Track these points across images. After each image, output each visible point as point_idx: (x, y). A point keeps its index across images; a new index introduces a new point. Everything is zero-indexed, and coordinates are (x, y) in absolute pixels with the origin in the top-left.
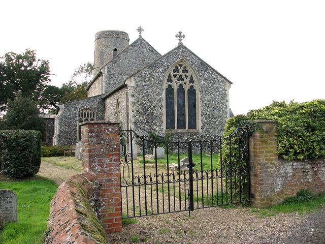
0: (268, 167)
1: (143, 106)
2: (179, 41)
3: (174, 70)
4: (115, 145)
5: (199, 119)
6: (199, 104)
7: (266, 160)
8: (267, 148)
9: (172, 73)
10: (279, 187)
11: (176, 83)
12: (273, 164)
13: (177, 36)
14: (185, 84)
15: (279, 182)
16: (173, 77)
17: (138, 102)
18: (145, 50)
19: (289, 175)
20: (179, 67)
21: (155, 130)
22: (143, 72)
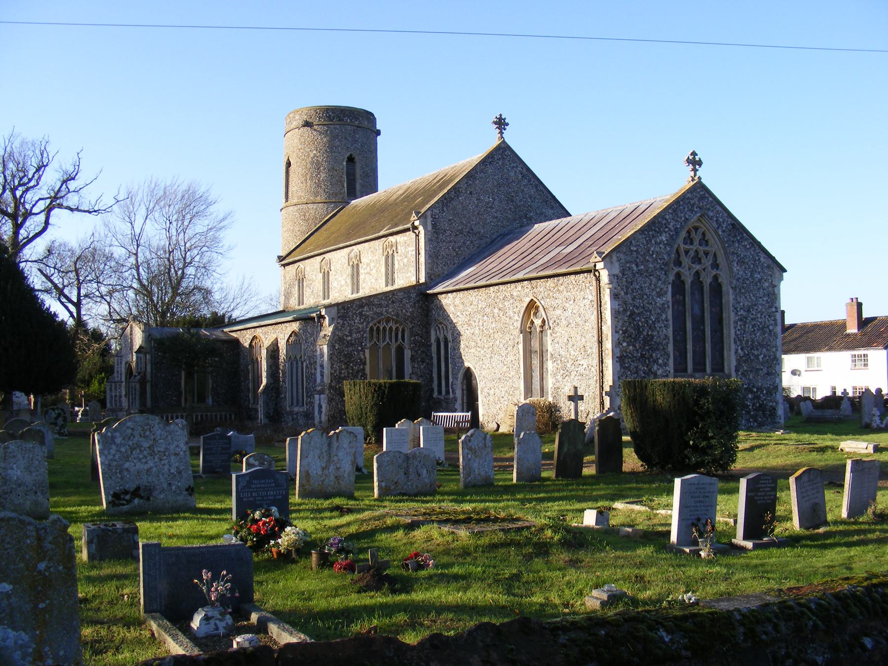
5: (730, 350)
6: (730, 317)
11: (689, 269)
16: (683, 254)
18: (512, 174)
20: (693, 234)
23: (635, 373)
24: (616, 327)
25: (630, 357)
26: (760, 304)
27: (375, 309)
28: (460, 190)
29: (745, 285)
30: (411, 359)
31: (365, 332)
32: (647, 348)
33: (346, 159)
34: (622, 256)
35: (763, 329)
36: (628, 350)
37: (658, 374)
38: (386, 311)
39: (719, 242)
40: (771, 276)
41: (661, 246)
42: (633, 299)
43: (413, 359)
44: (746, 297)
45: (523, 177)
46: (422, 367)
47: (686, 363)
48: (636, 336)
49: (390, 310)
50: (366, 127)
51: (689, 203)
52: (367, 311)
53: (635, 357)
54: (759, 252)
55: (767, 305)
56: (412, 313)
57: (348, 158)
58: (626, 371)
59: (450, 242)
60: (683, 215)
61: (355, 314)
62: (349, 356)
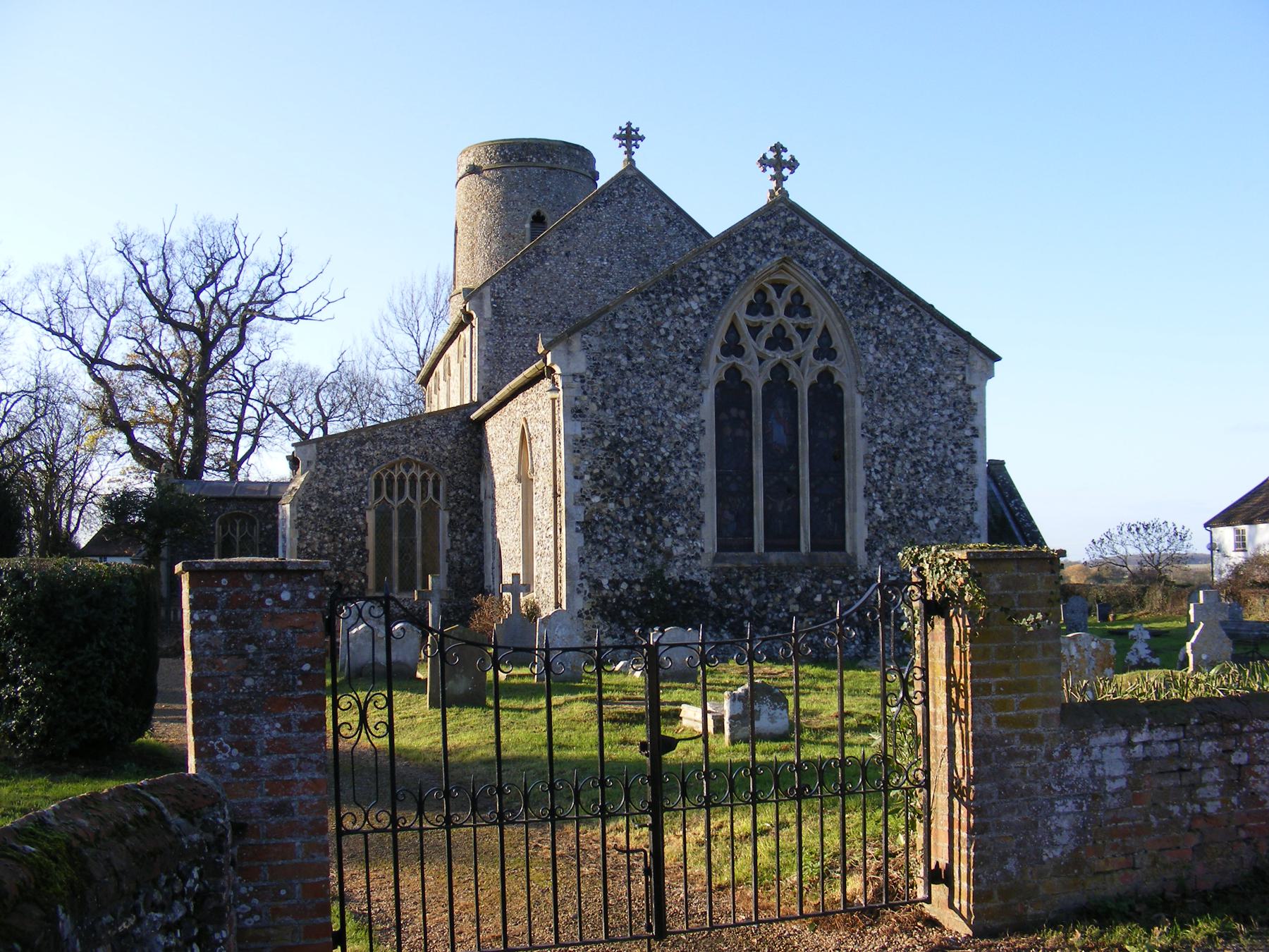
0: (1013, 755)
1: (620, 454)
2: (773, 184)
3: (751, 304)
4: (307, 660)
5: (855, 510)
6: (857, 448)
7: (1001, 722)
8: (1006, 670)
9: (744, 320)
10: (1062, 839)
11: (761, 360)
12: (1038, 739)
13: (764, 162)
14: (798, 361)
15: (1065, 815)
16: (746, 338)
17: (600, 438)
19: (1111, 786)
20: (772, 293)
21: (668, 555)
22: (621, 314)
23: (621, 552)
24: (577, 468)
25: (608, 524)
26: (933, 423)
27: (384, 447)
28: (548, 250)
29: (896, 388)
30: (449, 526)
31: (366, 484)
32: (650, 505)
33: (530, 219)
34: (595, 341)
35: (939, 469)
36: (604, 511)
37: (675, 553)
38: (404, 450)
39: (830, 309)
40: (963, 369)
41: (687, 319)
42: (618, 418)
43: (453, 525)
44: (897, 410)
45: (668, 223)
46: (469, 539)
47: (751, 534)
48: (624, 484)
49: (412, 448)
50: (566, 167)
51: (760, 238)
52: (370, 449)
53: (622, 523)
54: (934, 325)
55: (952, 423)
56: (452, 452)
57: (534, 217)
58: (600, 548)
59: (527, 335)
60: (743, 260)
61: (349, 454)
62: (338, 521)
